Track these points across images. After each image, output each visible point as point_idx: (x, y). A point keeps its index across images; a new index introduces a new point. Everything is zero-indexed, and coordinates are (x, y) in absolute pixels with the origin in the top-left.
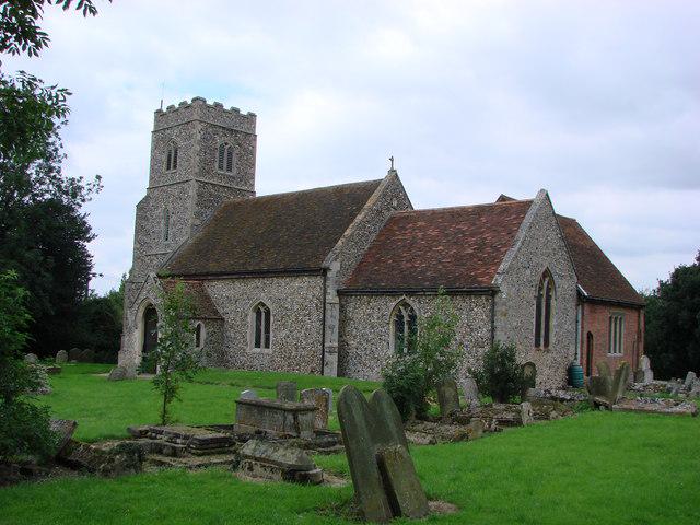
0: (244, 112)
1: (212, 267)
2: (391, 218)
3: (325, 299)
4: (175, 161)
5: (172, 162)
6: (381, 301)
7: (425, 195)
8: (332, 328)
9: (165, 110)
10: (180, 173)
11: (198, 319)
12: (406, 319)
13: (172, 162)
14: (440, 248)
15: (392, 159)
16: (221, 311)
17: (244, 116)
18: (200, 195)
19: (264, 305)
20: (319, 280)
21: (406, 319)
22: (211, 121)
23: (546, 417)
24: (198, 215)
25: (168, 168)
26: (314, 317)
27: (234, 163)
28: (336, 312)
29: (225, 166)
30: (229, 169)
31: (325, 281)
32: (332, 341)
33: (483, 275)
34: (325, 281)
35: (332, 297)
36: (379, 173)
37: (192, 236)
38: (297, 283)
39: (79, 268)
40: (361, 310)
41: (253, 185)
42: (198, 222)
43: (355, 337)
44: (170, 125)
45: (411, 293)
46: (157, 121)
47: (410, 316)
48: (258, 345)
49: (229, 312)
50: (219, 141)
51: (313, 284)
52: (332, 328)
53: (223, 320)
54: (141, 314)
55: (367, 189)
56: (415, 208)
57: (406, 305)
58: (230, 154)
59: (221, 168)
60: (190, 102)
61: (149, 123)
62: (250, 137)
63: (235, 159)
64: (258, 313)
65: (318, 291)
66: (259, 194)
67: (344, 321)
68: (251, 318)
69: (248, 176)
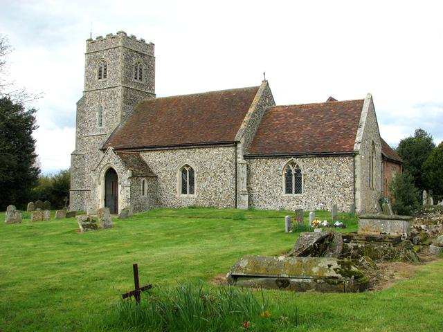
0: (148, 42)
1: (145, 142)
2: (266, 111)
3: (236, 161)
4: (106, 73)
5: (102, 74)
6: (275, 161)
7: (283, 97)
8: (243, 179)
9: (94, 39)
10: (110, 81)
11: (143, 177)
12: (293, 172)
13: (102, 74)
14: (309, 128)
15: (264, 74)
16: (155, 171)
17: (147, 45)
18: (125, 96)
19: (187, 166)
20: (232, 149)
21: (293, 172)
22: (129, 47)
23: (87, 230)
24: (124, 109)
25: (100, 78)
26: (229, 173)
27: (143, 77)
28: (245, 169)
29: (138, 78)
30: (141, 79)
31: (236, 150)
32: (243, 186)
33: (344, 144)
34: (235, 152)
35: (240, 160)
36: (255, 82)
37: (122, 123)
38: (214, 151)
39: (25, 148)
40: (260, 167)
41: (154, 90)
42: (124, 114)
43: (257, 185)
44: (96, 48)
45: (297, 156)
46: (88, 46)
47: (296, 170)
48: (184, 191)
49: (160, 171)
50: (135, 61)
51: (227, 152)
52: (243, 179)
53: (157, 177)
54: (103, 175)
55: (255, 90)
56: (277, 104)
57: (293, 164)
58: (141, 69)
59: (136, 78)
60: (104, 37)
61: (83, 48)
62: (151, 58)
63: (144, 73)
64: (184, 171)
65: (231, 156)
66: (157, 97)
67: (249, 175)
68: (179, 175)
69: (151, 85)
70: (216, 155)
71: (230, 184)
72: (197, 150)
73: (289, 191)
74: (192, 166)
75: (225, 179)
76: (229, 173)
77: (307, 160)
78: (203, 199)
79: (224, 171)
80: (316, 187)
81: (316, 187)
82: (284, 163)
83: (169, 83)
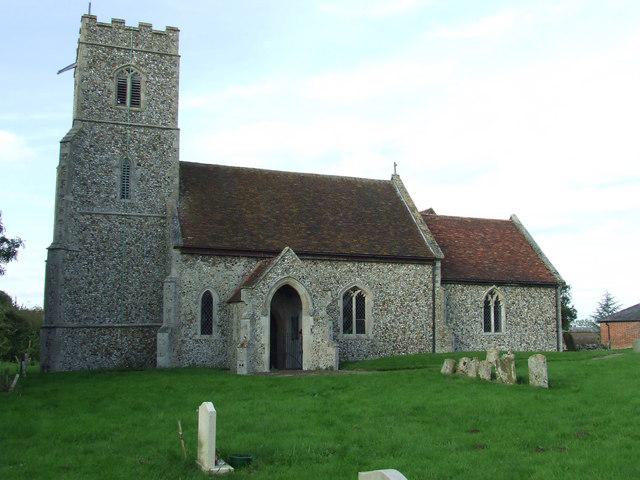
26: (422, 302)
38: (402, 270)
41: (177, 123)
45: (500, 284)
70: (405, 275)
71: (424, 318)
72: (375, 265)
73: (487, 328)
74: (366, 289)
75: (416, 311)
76: (422, 302)
77: (509, 289)
78: (384, 341)
79: (416, 300)
80: (518, 324)
81: (518, 324)
82: (484, 292)
83: (224, 124)
